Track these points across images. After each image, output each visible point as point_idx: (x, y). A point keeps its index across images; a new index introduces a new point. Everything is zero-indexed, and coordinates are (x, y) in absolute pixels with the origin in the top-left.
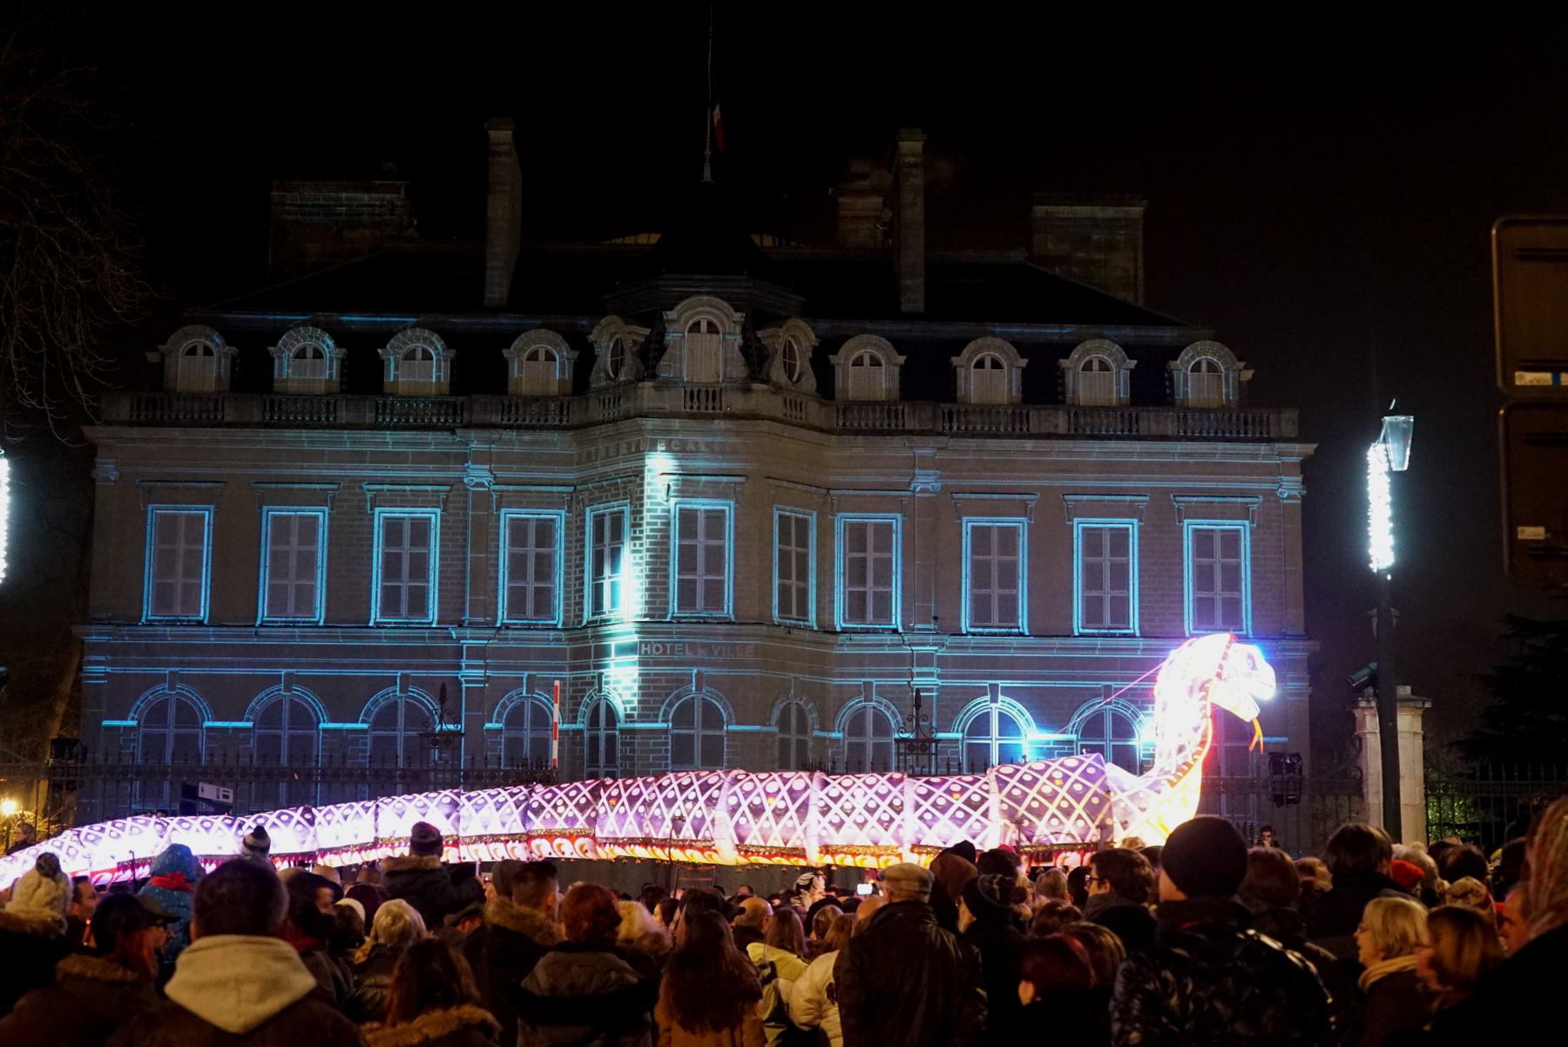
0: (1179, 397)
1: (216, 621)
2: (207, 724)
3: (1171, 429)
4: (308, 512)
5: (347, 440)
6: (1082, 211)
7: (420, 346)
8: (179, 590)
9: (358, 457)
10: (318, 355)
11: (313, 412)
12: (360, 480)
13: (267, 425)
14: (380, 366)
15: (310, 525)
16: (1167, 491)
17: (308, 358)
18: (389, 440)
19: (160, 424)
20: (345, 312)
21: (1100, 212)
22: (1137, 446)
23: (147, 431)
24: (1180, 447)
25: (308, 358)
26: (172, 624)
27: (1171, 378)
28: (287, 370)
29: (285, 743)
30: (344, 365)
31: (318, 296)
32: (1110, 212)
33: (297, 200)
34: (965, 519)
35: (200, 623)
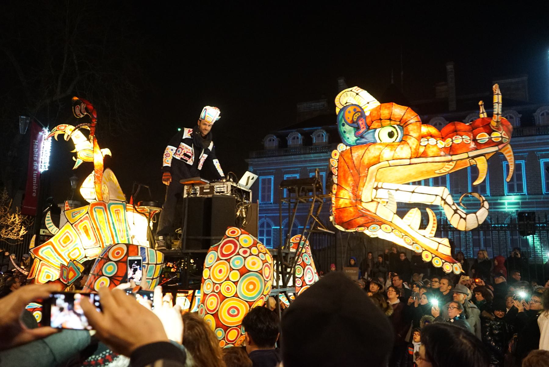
0: (537, 123)
1: (275, 202)
2: (273, 227)
3: (534, 132)
4: (269, 177)
5: (302, 157)
6: (509, 80)
7: (321, 133)
8: (266, 196)
9: (306, 161)
10: (298, 138)
11: (297, 151)
12: (306, 167)
13: (285, 156)
14: (311, 139)
15: (270, 180)
16: (533, 151)
17: (295, 139)
18: (312, 156)
19: (262, 157)
20: (304, 127)
21: (513, 80)
22: (523, 139)
23: (259, 159)
24: (537, 137)
25: (295, 139)
26: (265, 204)
27: (534, 119)
28: (290, 142)
29: (265, 235)
30: (303, 140)
31: (298, 126)
32: (517, 80)
33: (303, 107)
34: (541, 160)
35: (271, 204)
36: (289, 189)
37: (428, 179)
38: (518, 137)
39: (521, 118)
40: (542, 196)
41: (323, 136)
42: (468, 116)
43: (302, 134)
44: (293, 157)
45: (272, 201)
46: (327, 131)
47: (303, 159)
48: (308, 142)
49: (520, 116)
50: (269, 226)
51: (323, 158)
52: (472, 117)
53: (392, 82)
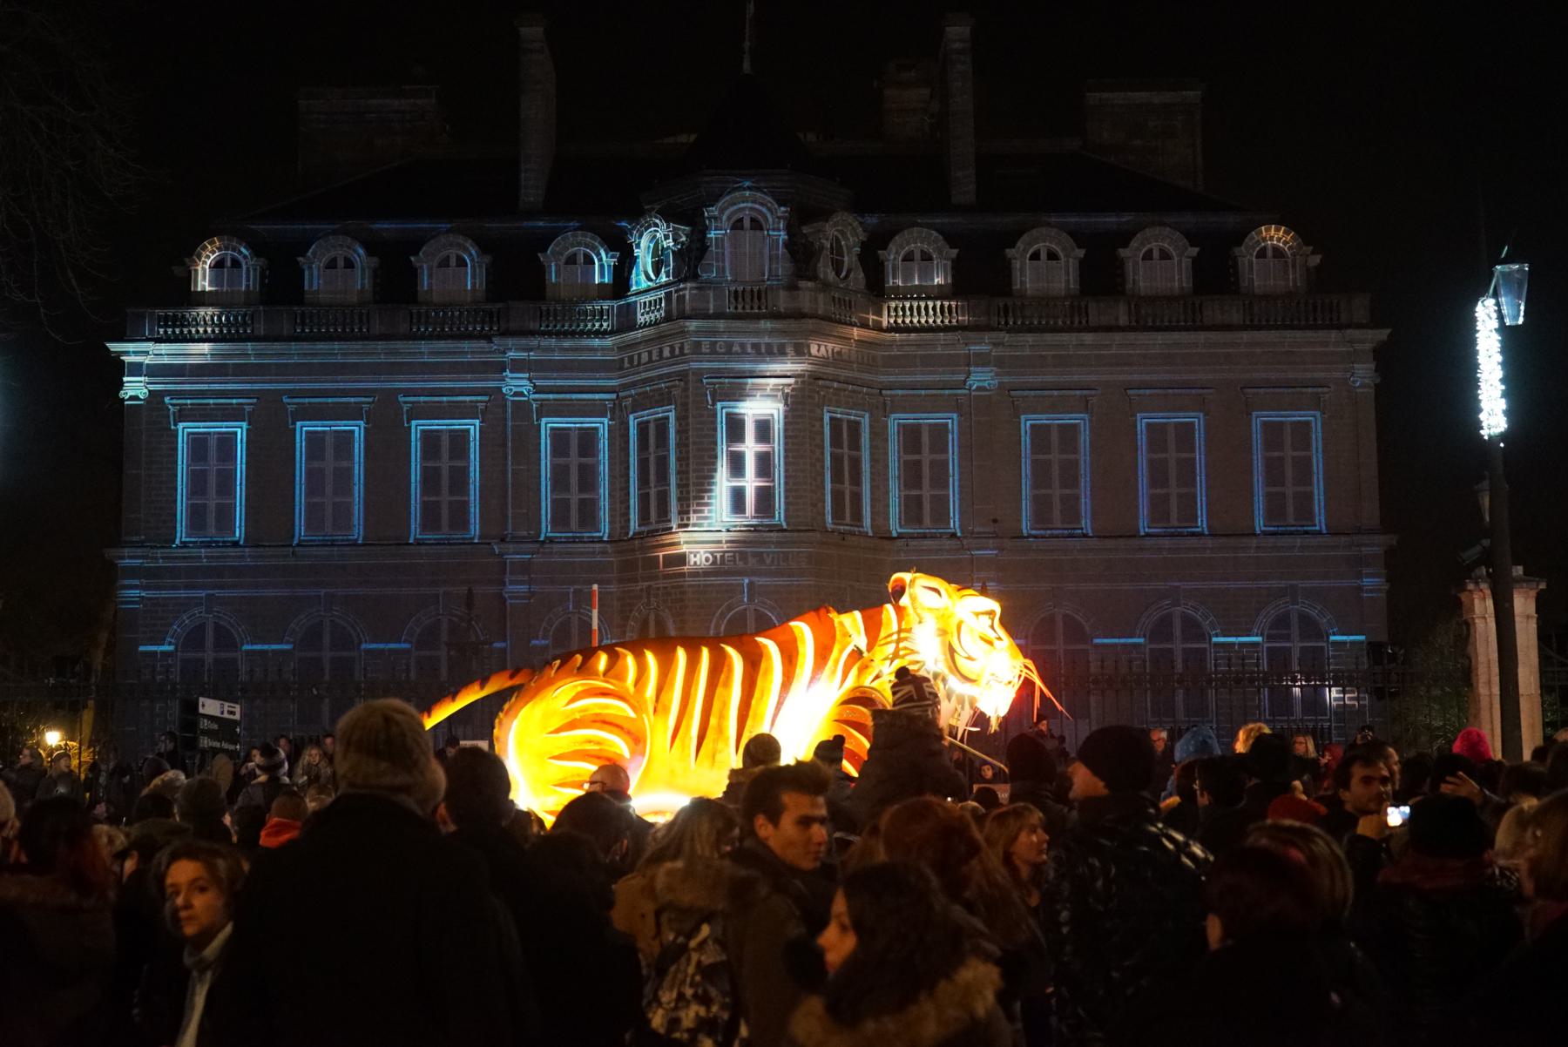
2: (246, 647)
5: (379, 352)
6: (1141, 96)
7: (453, 253)
10: (349, 264)
14: (413, 273)
15: (227, 441)
18: (426, 351)
21: (1157, 98)
26: (207, 545)
28: (315, 279)
35: (236, 544)
36: (680, 526)
37: (648, 422)
38: (1186, 329)
39: (1196, 262)
40: (1254, 542)
41: (462, 263)
42: (1025, 237)
43: (370, 251)
44: (336, 345)
45: (239, 533)
46: (484, 246)
47: (383, 359)
48: (396, 287)
49: (1194, 251)
50: (1311, 629)
51: (469, 358)
52: (1036, 241)
53: (746, 66)
